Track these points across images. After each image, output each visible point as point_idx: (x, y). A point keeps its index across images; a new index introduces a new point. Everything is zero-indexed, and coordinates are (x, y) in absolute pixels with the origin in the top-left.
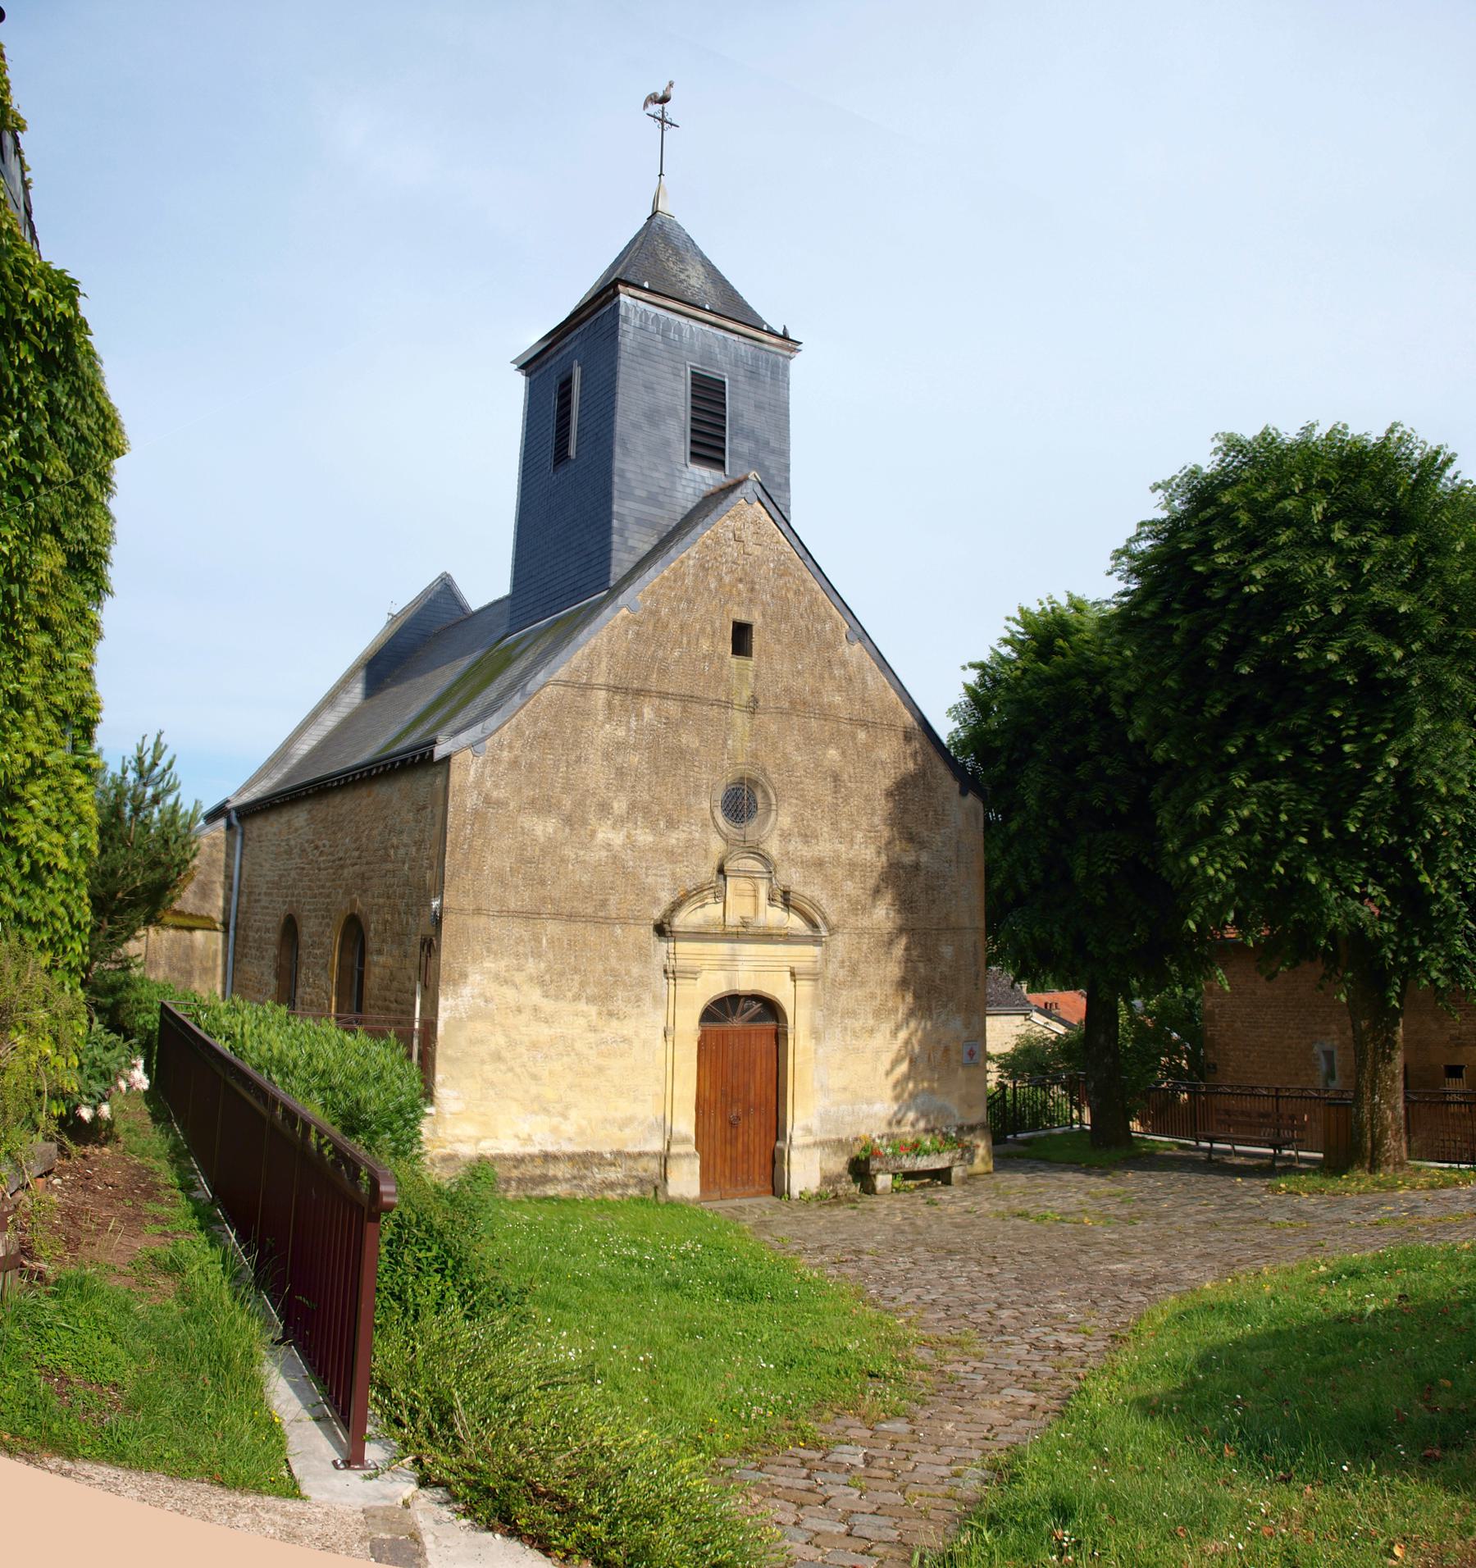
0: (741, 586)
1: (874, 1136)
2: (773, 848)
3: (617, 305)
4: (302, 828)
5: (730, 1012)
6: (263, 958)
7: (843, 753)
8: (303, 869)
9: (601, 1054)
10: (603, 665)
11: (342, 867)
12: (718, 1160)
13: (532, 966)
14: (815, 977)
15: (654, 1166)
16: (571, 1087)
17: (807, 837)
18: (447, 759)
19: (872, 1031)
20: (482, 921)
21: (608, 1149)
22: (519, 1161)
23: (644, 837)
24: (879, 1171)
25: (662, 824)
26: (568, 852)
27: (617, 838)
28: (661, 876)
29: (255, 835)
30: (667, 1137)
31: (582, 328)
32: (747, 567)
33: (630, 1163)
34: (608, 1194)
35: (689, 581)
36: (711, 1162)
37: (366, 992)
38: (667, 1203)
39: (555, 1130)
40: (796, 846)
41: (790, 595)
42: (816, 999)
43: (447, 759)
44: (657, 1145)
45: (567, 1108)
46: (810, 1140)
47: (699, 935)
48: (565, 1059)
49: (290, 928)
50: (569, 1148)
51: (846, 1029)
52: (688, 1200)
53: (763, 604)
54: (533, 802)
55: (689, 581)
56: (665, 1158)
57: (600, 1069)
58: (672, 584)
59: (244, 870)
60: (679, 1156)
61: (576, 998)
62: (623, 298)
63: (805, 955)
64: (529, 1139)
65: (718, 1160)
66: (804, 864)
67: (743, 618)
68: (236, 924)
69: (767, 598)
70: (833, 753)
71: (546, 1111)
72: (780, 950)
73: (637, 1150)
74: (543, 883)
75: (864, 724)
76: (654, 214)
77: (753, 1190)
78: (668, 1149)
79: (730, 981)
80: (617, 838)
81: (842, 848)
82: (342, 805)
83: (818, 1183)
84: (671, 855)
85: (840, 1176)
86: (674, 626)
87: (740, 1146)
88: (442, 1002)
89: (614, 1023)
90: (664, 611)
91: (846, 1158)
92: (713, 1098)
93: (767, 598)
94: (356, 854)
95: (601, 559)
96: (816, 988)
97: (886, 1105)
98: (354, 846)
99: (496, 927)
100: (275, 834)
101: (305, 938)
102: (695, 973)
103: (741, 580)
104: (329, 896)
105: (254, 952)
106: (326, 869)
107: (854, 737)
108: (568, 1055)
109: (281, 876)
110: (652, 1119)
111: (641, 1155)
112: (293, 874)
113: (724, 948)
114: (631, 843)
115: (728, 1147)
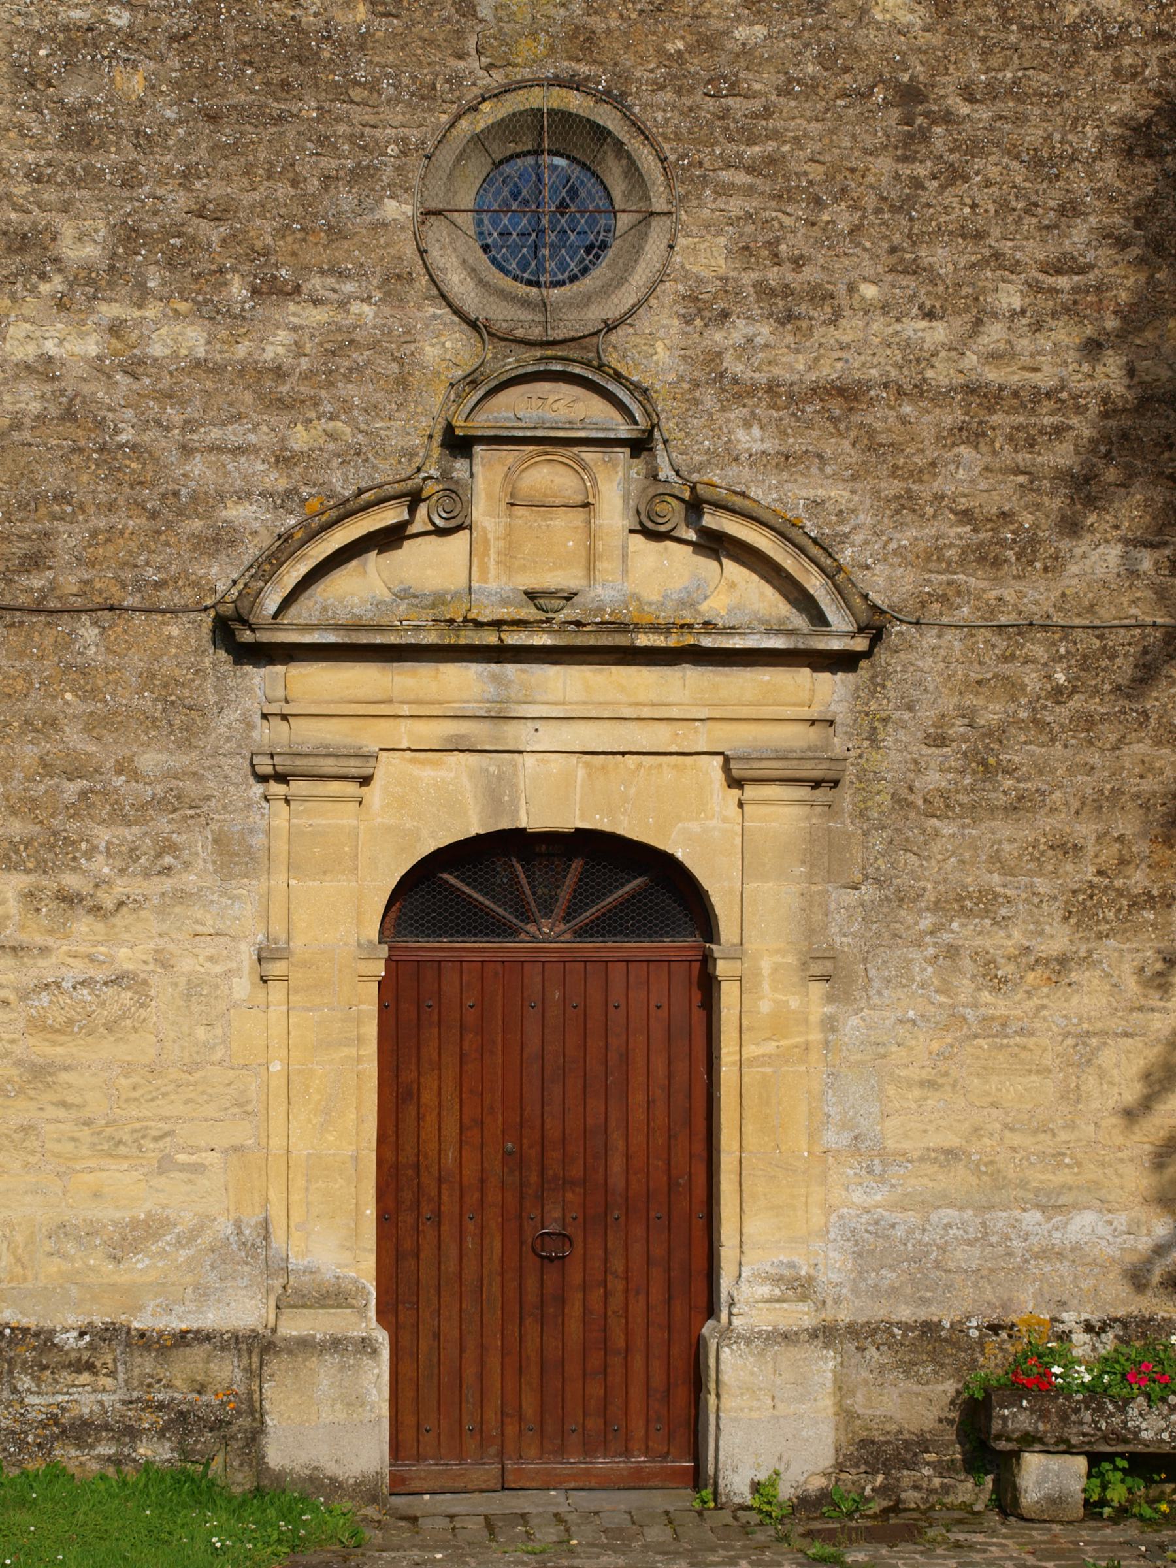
1: (1070, 1318)
5: (560, 909)
12: (494, 1362)
21: (75, 1319)
24: (1029, 1440)
25: (237, 289)
28: (241, 450)
33: (146, 1364)
34: (68, 1455)
36: (470, 1372)
38: (258, 1491)
46: (802, 1316)
52: (335, 1487)
65: (494, 1362)
73: (176, 1323)
77: (620, 1465)
83: (826, 1460)
85: (923, 1443)
87: (574, 1327)
89: (83, 925)
91: (950, 1387)
92: (471, 1173)
97: (1121, 1220)
111: (183, 1339)
115: (532, 1328)
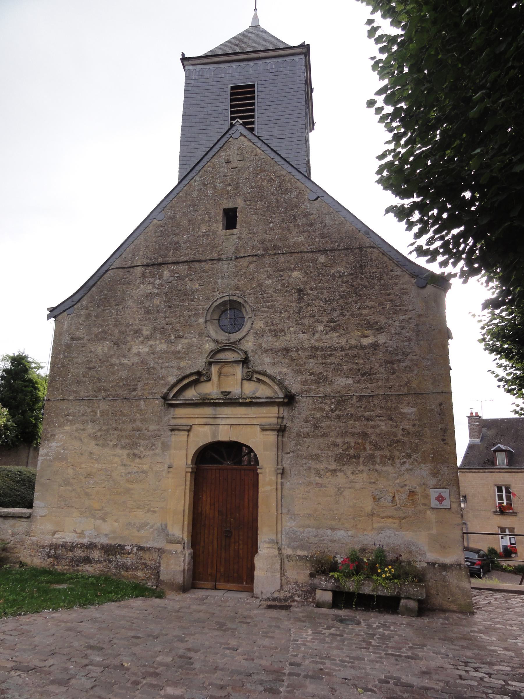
7: (306, 273)
13: (91, 428)
20: (64, 405)
22: (72, 547)
23: (161, 347)
25: (173, 337)
26: (115, 360)
27: (144, 349)
35: (195, 194)
39: (97, 529)
40: (268, 341)
50: (104, 541)
51: (309, 468)
53: (244, 194)
55: (195, 194)
57: (128, 491)
58: (184, 199)
61: (115, 446)
64: (82, 534)
66: (274, 351)
70: (296, 274)
71: (94, 517)
72: (252, 411)
74: (99, 380)
79: (214, 434)
80: (144, 349)
84: (178, 356)
99: (72, 408)
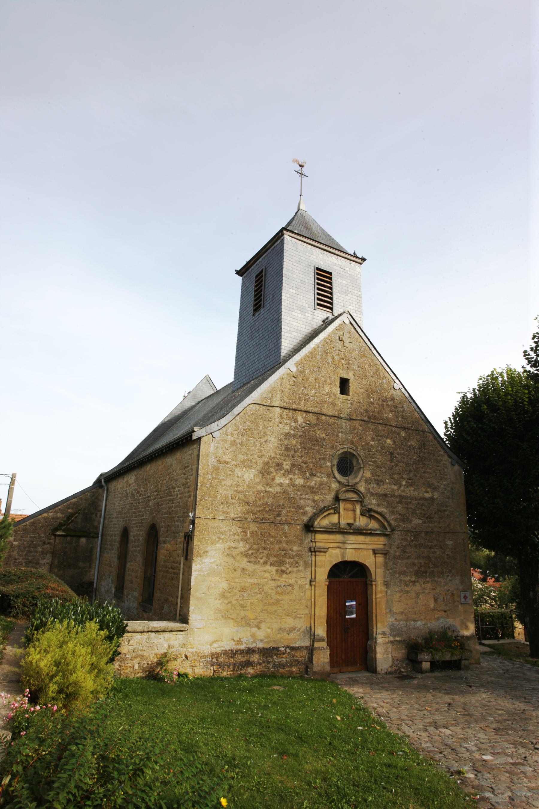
0: (343, 361)
2: (362, 488)
3: (283, 240)
4: (132, 483)
6: (113, 550)
7: (394, 442)
8: (132, 503)
9: (277, 593)
10: (278, 396)
11: (149, 501)
14: (385, 554)
15: (305, 653)
16: (262, 611)
17: (379, 482)
18: (199, 439)
19: (414, 582)
20: (216, 523)
23: (299, 481)
29: (112, 490)
30: (312, 637)
31: (267, 253)
32: (346, 353)
37: (158, 564)
41: (367, 366)
42: (386, 564)
43: (199, 439)
44: (306, 643)
45: (260, 622)
47: (328, 531)
48: (259, 596)
49: (125, 533)
50: (260, 645)
54: (243, 462)
55: (319, 357)
56: (311, 650)
59: (107, 507)
60: (319, 648)
61: (265, 563)
62: (285, 236)
63: (379, 542)
67: (345, 376)
68: (102, 533)
69: (356, 367)
70: (389, 441)
75: (404, 428)
76: (299, 210)
78: (313, 645)
79: (343, 556)
81: (396, 487)
82: (151, 469)
84: (313, 490)
86: (312, 379)
88: (194, 565)
90: (307, 371)
93: (356, 367)
94: (156, 493)
95: (276, 350)
96: (385, 558)
98: (155, 490)
100: (121, 488)
101: (131, 538)
102: (325, 550)
103: (343, 359)
104: (143, 516)
105: (109, 546)
106: (142, 503)
107: (399, 434)
108: (260, 593)
109: (122, 508)
110: (304, 628)
112: (128, 507)
113: (339, 537)
114: (292, 484)
